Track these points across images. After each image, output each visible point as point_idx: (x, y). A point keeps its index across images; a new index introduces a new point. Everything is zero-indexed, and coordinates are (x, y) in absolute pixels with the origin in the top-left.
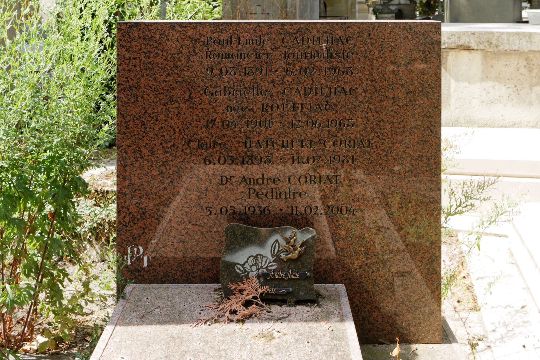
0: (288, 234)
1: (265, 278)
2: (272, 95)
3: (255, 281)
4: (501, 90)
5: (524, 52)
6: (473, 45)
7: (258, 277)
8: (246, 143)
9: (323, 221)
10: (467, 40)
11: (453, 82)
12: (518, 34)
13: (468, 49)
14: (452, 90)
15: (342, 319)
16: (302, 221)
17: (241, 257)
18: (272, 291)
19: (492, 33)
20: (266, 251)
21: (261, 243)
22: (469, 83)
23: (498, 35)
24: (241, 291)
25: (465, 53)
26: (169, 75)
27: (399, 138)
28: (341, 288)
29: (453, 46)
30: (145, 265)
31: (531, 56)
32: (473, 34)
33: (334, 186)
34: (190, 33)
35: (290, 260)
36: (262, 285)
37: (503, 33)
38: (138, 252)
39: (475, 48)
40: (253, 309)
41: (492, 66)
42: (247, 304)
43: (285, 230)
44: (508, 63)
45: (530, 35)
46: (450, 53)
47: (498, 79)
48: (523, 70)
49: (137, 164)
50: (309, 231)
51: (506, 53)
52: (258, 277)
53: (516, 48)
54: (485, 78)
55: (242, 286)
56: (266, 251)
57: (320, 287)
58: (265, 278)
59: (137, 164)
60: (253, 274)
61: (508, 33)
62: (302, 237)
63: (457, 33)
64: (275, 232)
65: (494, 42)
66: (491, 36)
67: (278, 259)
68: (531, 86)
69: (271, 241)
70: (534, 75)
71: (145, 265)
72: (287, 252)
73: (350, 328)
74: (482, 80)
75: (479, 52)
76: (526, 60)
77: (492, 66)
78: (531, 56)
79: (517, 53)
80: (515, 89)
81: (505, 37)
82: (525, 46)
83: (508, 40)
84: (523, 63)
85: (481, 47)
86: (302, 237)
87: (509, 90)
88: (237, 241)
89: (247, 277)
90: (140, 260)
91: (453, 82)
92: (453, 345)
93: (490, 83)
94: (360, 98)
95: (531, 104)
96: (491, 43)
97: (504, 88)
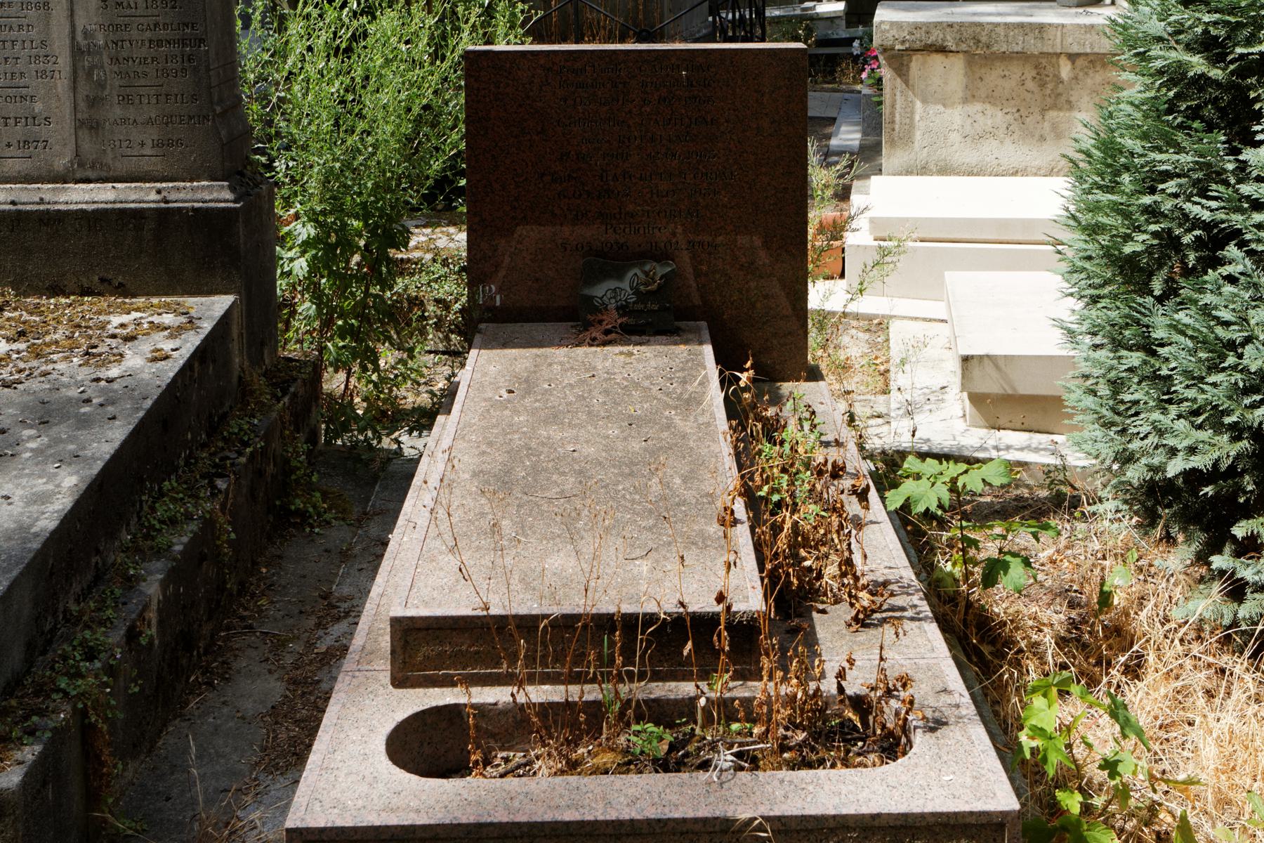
0: (647, 268)
1: (623, 309)
2: (629, 126)
3: (615, 314)
4: (995, 117)
5: (1032, 55)
6: (950, 44)
7: (617, 309)
8: (601, 177)
9: (685, 257)
10: (941, 36)
11: (918, 104)
12: (1021, 26)
13: (942, 50)
14: (917, 118)
15: (701, 343)
16: (661, 256)
17: (600, 291)
18: (632, 321)
19: (980, 25)
20: (625, 285)
21: (620, 277)
22: (944, 106)
23: (990, 27)
24: (600, 322)
25: (938, 58)
26: (520, 106)
27: (764, 170)
28: (704, 324)
29: (918, 45)
30: (498, 303)
31: (1044, 61)
32: (951, 26)
33: (695, 220)
34: (542, 62)
35: (648, 292)
36: (621, 316)
37: (998, 25)
38: (490, 289)
39: (953, 48)
40: (613, 336)
41: (981, 79)
42: (607, 332)
43: (644, 264)
44: (1007, 73)
45: (1041, 27)
46: (914, 58)
47: (991, 99)
48: (1030, 85)
49: (488, 200)
50: (669, 265)
51: (1005, 57)
52: (617, 309)
53: (1018, 48)
54: (970, 96)
55: (600, 317)
56: (625, 285)
57: (682, 324)
58: (623, 309)
59: (488, 200)
60: (612, 306)
61: (1006, 24)
62: (661, 270)
63: (924, 24)
64: (634, 266)
65: (984, 39)
66: (979, 29)
67: (637, 292)
68: (1043, 111)
69: (630, 274)
70: (1048, 92)
71: (498, 303)
72: (646, 284)
73: (708, 350)
74: (965, 101)
75: (961, 55)
76: (1036, 67)
77: (981, 79)
78: (1044, 61)
79: (1023, 56)
80: (1017, 115)
81: (1001, 31)
82: (1033, 45)
83: (1006, 36)
84: (1030, 73)
85: (964, 47)
86: (661, 270)
87: (1008, 117)
88: (595, 275)
89: (606, 309)
90: (493, 299)
91: (918, 104)
92: (821, 383)
93: (978, 106)
94: (722, 128)
95: (1042, 138)
96: (979, 41)
97: (1000, 114)
